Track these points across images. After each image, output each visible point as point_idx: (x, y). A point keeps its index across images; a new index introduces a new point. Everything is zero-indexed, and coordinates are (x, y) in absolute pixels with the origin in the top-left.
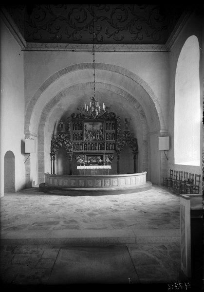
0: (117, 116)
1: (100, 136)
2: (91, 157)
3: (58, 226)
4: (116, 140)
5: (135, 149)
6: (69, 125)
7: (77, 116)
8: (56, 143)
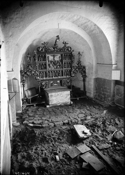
1: (60, 66)
4: (72, 68)
7: (42, 50)
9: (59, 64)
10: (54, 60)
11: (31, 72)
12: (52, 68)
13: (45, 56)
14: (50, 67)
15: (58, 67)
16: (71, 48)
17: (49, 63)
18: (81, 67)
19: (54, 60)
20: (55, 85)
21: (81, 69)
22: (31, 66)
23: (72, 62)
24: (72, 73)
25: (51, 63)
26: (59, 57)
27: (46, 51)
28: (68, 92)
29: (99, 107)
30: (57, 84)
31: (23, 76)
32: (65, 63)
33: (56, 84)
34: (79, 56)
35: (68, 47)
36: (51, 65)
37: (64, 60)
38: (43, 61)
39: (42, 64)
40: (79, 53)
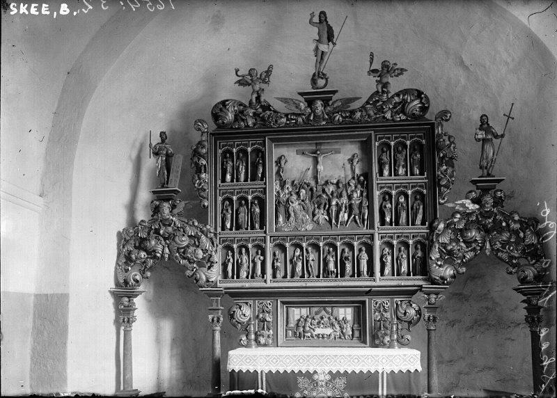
0: (434, 109)
1: (350, 208)
2: (305, 311)
3: (219, 182)
4: (432, 229)
5: (530, 273)
6: (201, 156)
7: (239, 116)
8: (141, 244)
9: (350, 197)
10: (316, 178)
11: (169, 238)
12: (305, 222)
13: (260, 154)
14: (288, 216)
15: (344, 216)
16: (419, 94)
17: (283, 197)
18: (508, 218)
19: (316, 172)
20: (319, 331)
21: (501, 230)
22: (174, 207)
23: (434, 183)
24: (435, 255)
25: (298, 194)
26: (351, 161)
27: (263, 119)
28: (231, 353)
29: (229, 205)
30: (332, 325)
31: (128, 259)
32: (386, 196)
33: (328, 331)
34: (485, 141)
35: (405, 92)
36: (295, 205)
37: (381, 174)
38: (246, 180)
39: (243, 199)
40: (484, 124)
